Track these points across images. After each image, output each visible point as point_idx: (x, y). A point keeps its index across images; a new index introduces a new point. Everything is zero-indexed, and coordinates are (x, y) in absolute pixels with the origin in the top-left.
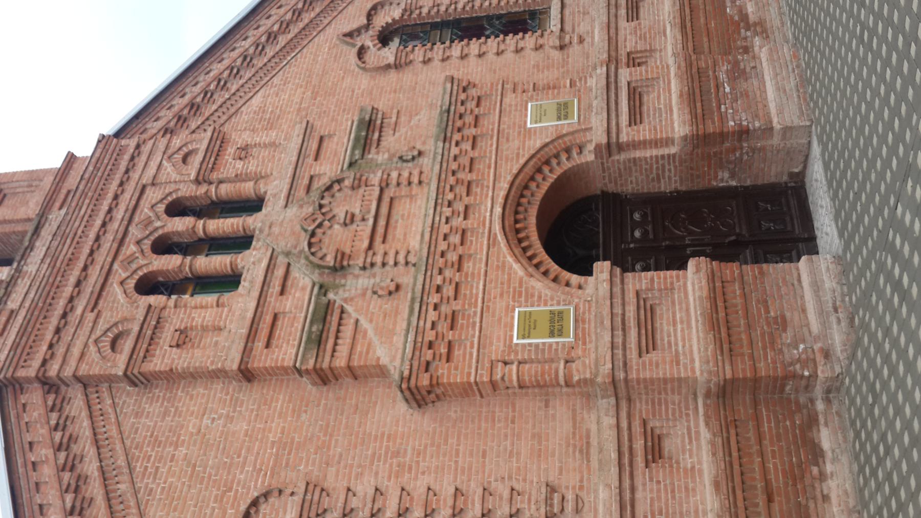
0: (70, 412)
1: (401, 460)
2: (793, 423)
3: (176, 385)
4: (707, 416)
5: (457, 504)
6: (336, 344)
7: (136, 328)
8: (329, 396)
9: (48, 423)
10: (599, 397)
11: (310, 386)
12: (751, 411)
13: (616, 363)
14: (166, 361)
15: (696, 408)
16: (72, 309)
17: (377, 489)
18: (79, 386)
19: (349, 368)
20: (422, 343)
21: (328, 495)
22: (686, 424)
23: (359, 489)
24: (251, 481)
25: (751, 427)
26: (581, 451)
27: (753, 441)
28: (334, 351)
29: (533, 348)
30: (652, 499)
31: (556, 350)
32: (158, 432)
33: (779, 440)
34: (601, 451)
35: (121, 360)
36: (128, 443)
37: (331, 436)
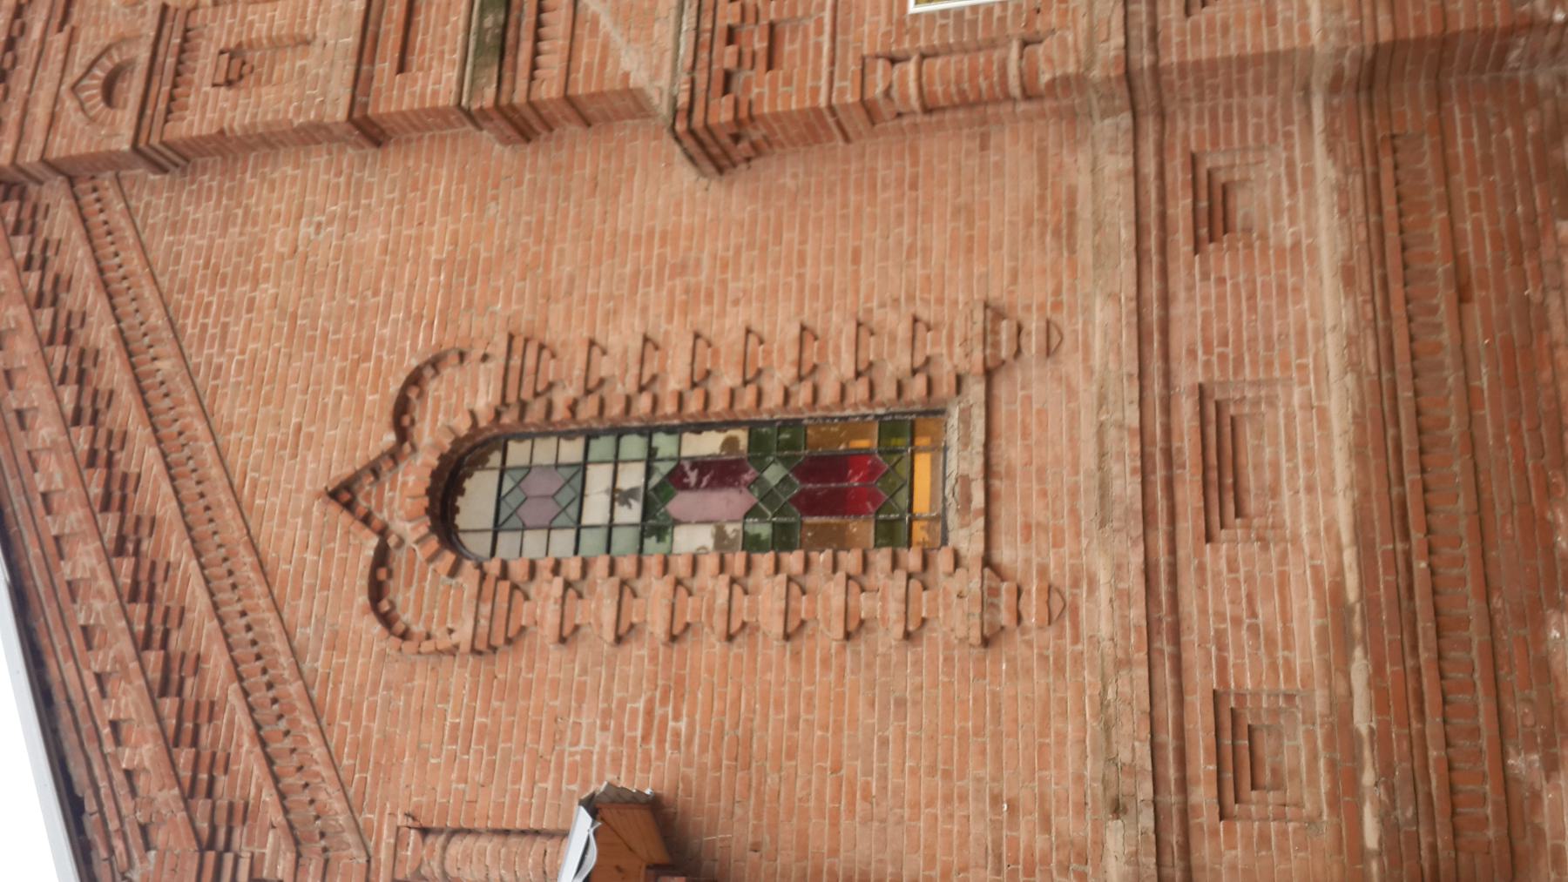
0: (51, 233)
1: (692, 280)
2: (1521, 132)
3: (239, 165)
4: (1332, 135)
5: (806, 355)
6: (536, 53)
7: (143, 55)
8: (536, 162)
9: (12, 256)
10: (1096, 114)
11: (498, 147)
12: (1428, 114)
13: (1133, 33)
14: (209, 115)
15: (1308, 119)
16: (23, 30)
17: (646, 339)
18: (59, 182)
19: (569, 100)
20: (713, 31)
21: (553, 356)
22: (1284, 155)
23: (614, 341)
24: (404, 339)
25: (1426, 147)
26: (1057, 233)
27: (1430, 176)
28: (534, 67)
29: (951, 21)
30: (1206, 317)
31: (1002, 20)
32: (218, 257)
33: (1488, 171)
34: (1098, 227)
35: (125, 118)
36: (164, 281)
37: (550, 243)
